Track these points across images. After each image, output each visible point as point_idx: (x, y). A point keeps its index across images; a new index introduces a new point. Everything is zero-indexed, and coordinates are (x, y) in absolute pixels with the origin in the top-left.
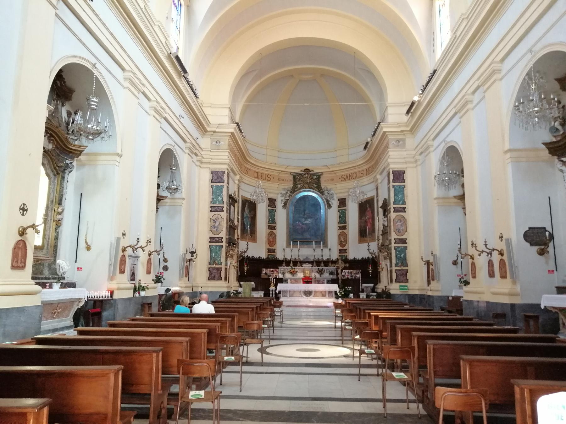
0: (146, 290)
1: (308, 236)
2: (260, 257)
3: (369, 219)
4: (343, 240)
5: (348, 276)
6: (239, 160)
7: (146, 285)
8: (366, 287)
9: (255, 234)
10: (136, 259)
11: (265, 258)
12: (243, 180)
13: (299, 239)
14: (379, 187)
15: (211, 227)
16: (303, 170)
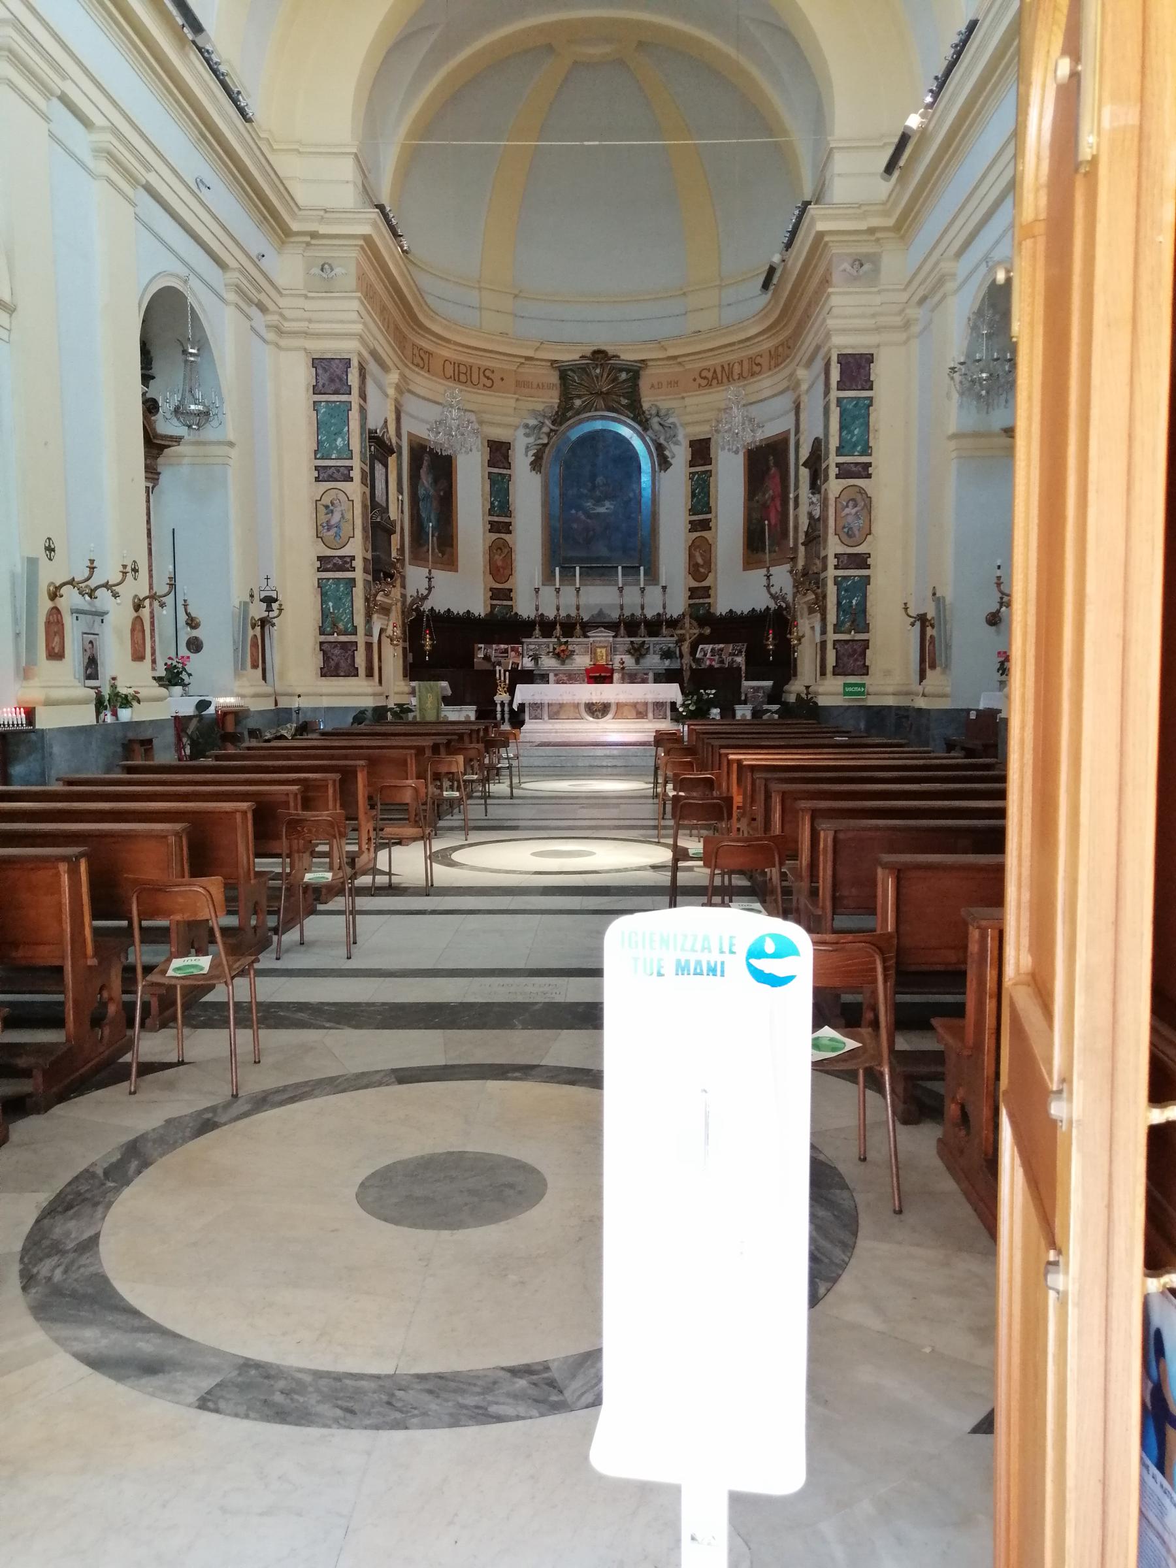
0: (135, 703)
1: (604, 552)
2: (468, 611)
3: (773, 498)
4: (700, 561)
5: (711, 660)
6: (397, 328)
7: (131, 691)
9: (452, 546)
10: (98, 619)
11: (483, 615)
12: (412, 387)
13: (579, 560)
16: (589, 355)
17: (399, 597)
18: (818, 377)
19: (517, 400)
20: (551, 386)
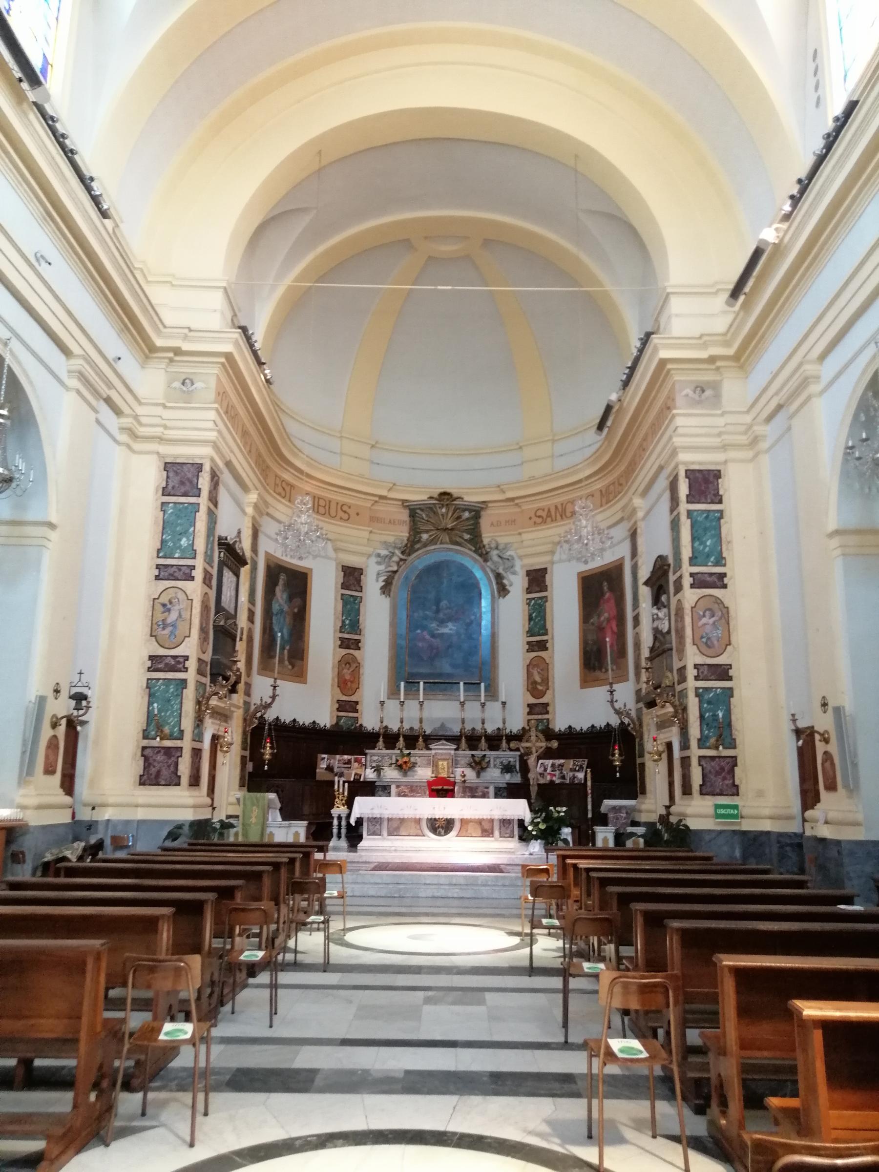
1: (447, 668)
2: (314, 722)
3: (608, 620)
4: (538, 678)
6: (259, 455)
8: (614, 809)
9: (302, 659)
11: (328, 726)
12: (271, 511)
13: (422, 676)
14: (639, 531)
15: (155, 626)
17: (241, 704)
18: (664, 491)
19: (371, 532)
20: (401, 522)
